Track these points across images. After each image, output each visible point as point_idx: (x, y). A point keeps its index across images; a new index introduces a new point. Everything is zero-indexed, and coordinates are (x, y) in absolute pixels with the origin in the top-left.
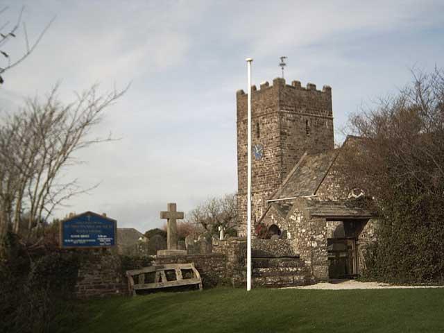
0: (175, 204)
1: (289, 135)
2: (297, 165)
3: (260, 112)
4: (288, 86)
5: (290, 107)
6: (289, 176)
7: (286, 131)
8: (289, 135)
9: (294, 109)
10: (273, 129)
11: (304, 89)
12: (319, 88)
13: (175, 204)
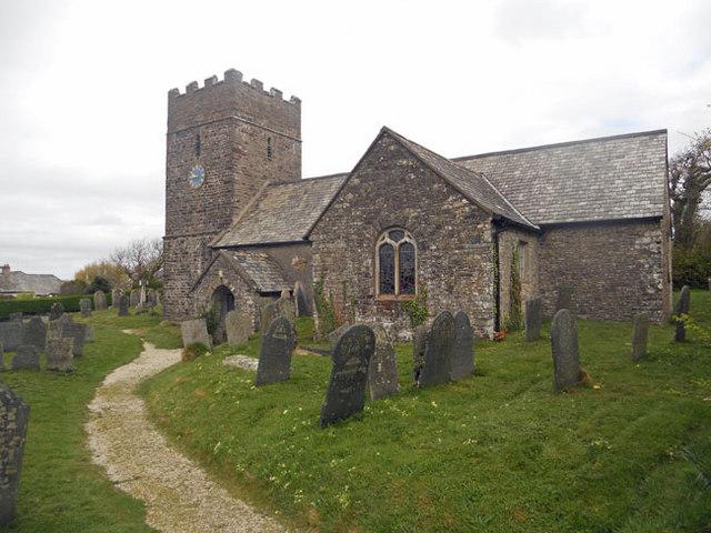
0: (385, 133)
2: (254, 199)
4: (245, 83)
6: (242, 213)
11: (266, 93)
12: (287, 97)
13: (385, 133)
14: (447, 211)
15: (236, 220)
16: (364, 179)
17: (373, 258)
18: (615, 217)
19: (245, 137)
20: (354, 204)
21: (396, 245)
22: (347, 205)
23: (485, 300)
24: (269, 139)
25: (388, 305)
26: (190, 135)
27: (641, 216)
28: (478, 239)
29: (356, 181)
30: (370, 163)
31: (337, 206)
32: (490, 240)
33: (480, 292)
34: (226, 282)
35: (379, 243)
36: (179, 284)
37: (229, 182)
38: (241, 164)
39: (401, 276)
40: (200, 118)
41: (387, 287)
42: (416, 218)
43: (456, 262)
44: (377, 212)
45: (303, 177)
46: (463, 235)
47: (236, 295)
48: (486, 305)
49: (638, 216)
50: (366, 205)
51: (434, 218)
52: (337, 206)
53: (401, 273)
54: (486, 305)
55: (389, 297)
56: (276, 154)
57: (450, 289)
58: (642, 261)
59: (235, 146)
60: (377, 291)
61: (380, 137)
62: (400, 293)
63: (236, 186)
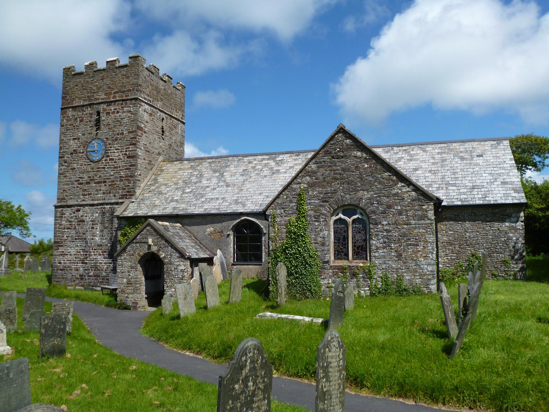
1: (145, 132)
3: (103, 96)
5: (148, 95)
6: (142, 185)
7: (143, 126)
8: (145, 132)
9: (151, 99)
10: (125, 120)
14: (396, 194)
15: (138, 192)
16: (320, 165)
17: (329, 231)
18: (492, 202)
19: (146, 117)
20: (312, 185)
21: (349, 220)
22: (303, 186)
23: (429, 264)
24: (163, 119)
25: (342, 269)
26: (89, 110)
27: (511, 202)
28: (424, 217)
29: (313, 166)
30: (327, 153)
31: (294, 186)
32: (433, 218)
33: (426, 257)
34: (154, 249)
35: (334, 218)
36: (73, 251)
37: (133, 157)
38: (143, 141)
39: (354, 246)
40: (102, 96)
41: (341, 253)
42: (369, 199)
43: (404, 235)
44: (335, 192)
45: (186, 156)
46: (410, 213)
47: (166, 261)
48: (430, 268)
49: (508, 202)
50: (324, 187)
51: (385, 200)
52: (294, 186)
53: (354, 243)
54: (430, 268)
55: (343, 263)
56: (167, 133)
57: (399, 256)
58: (511, 235)
59: (139, 124)
60: (332, 258)
61: (337, 133)
62: (353, 259)
63: (139, 161)
